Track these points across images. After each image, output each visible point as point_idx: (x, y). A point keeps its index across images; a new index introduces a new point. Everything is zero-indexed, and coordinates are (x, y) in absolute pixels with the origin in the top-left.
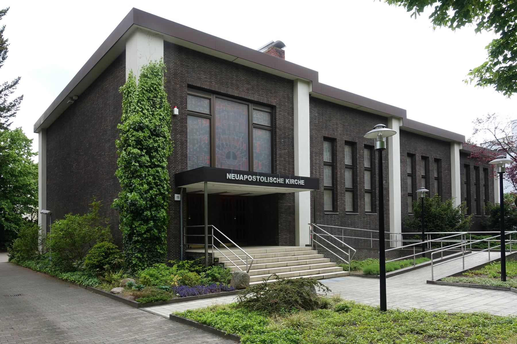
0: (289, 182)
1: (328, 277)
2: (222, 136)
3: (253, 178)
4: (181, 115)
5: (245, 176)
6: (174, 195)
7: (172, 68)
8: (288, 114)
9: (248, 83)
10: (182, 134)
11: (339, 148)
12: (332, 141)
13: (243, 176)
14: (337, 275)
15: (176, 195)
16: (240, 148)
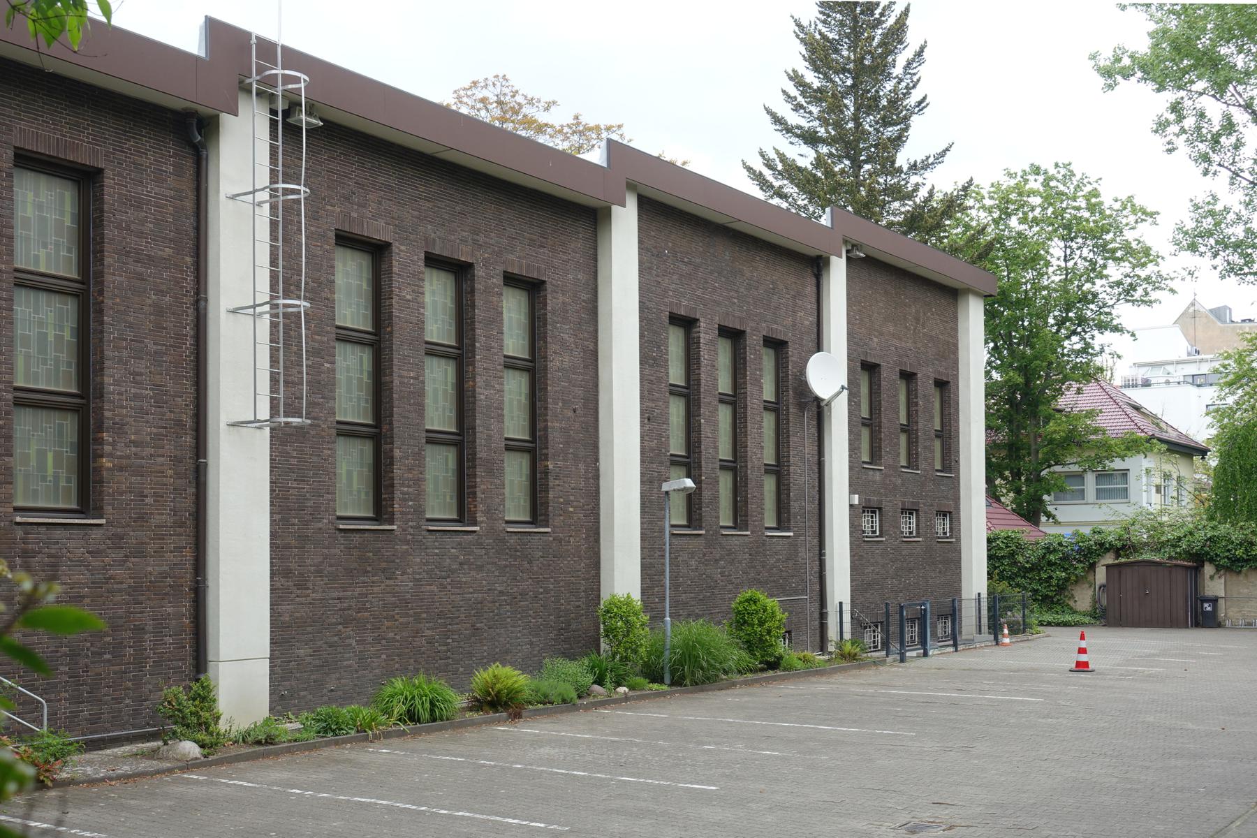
11: (750, 356)
12: (687, 323)
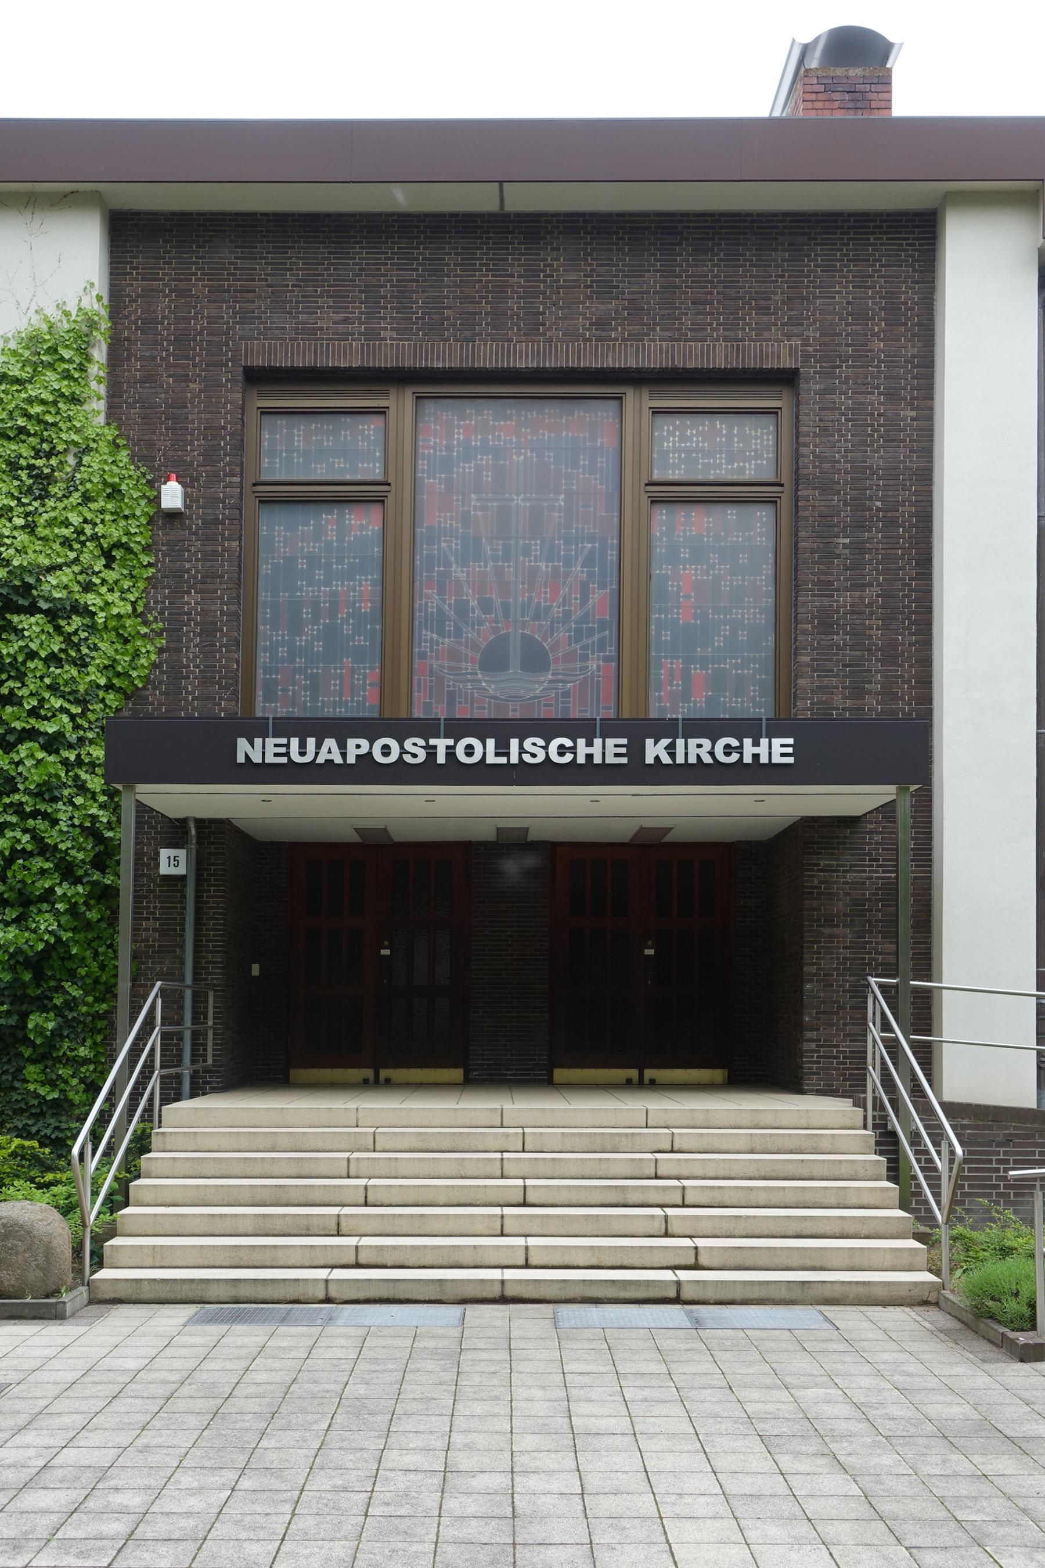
0: (672, 755)
1: (719, 1296)
2: (458, 572)
3: (403, 751)
4: (204, 508)
5: (351, 743)
6: (158, 854)
7: (164, 318)
8: (892, 395)
9: (605, 290)
10: (211, 587)
13: (342, 746)
14: (813, 1293)
15: (164, 853)
16: (567, 615)
